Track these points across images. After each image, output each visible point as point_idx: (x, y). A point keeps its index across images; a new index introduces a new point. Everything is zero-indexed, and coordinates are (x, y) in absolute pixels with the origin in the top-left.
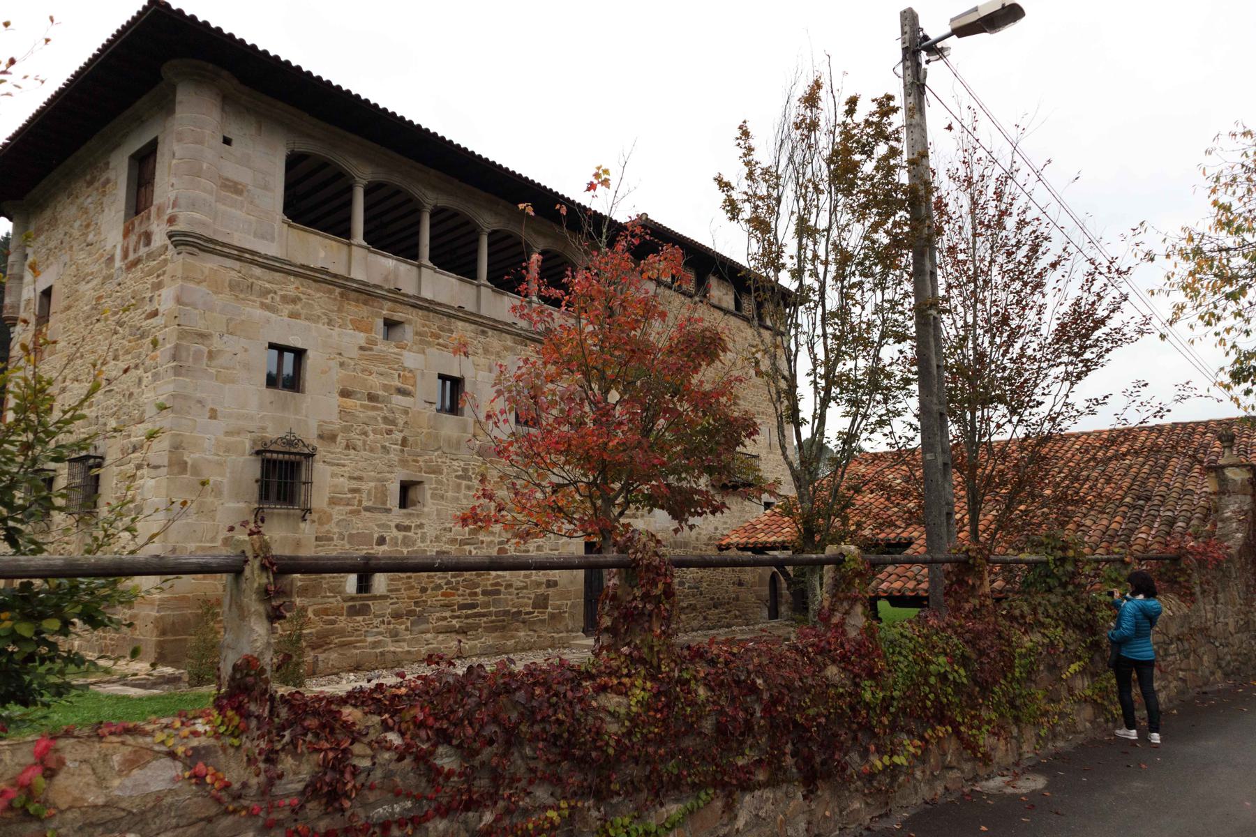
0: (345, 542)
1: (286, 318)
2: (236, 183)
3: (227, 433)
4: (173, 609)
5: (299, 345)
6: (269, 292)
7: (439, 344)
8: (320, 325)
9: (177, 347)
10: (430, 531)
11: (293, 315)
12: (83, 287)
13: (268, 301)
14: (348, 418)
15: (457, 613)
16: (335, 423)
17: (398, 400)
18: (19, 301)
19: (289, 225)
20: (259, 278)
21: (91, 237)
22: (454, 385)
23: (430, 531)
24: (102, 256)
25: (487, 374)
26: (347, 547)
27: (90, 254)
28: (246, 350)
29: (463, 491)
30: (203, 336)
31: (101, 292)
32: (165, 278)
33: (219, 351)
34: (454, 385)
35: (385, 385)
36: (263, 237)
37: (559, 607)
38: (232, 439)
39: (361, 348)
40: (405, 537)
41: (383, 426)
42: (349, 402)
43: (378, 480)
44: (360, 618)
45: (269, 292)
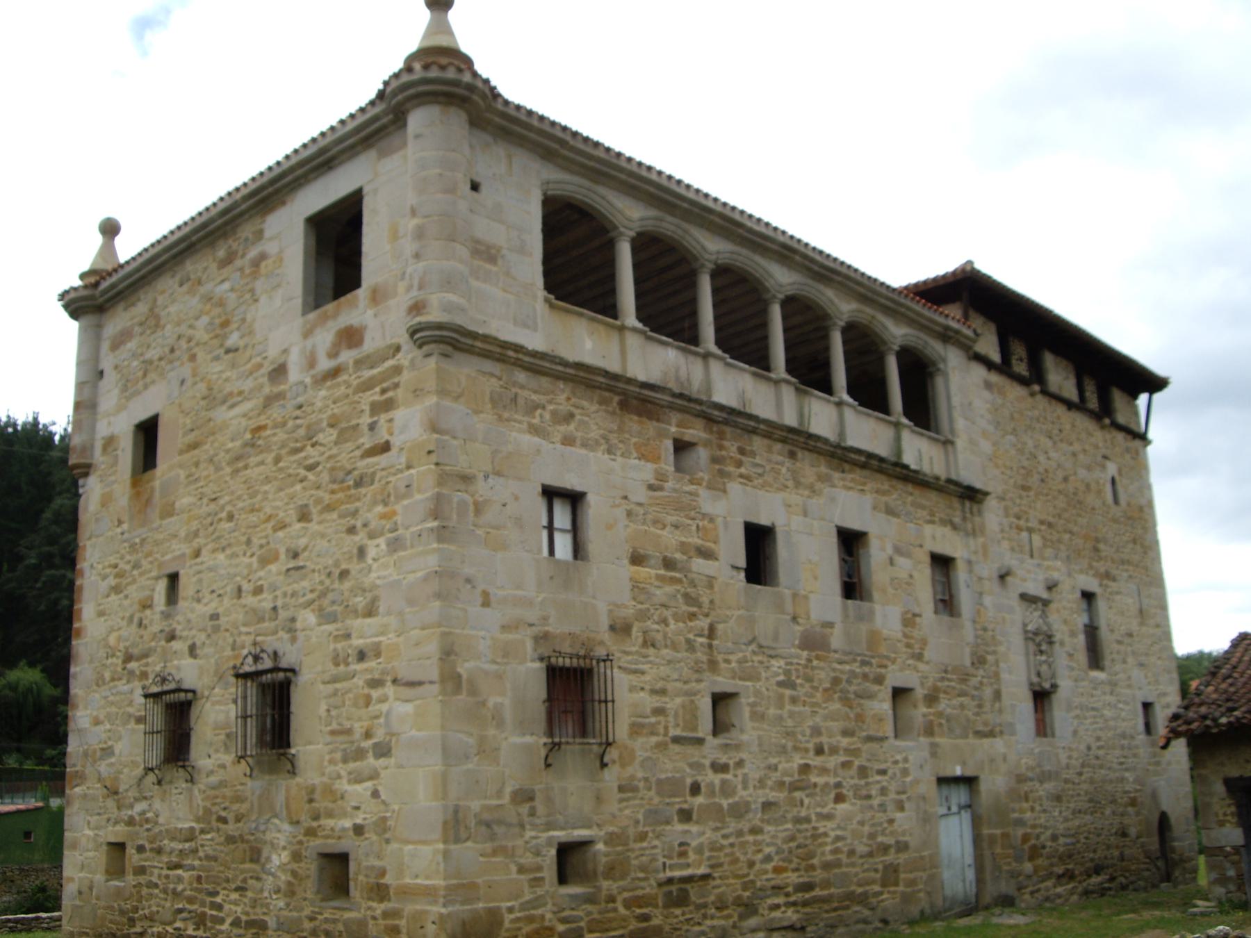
0: (652, 793)
1: (558, 446)
2: (489, 247)
3: (505, 628)
4: (463, 903)
5: (579, 488)
6: (537, 406)
7: (741, 476)
8: (599, 454)
9: (439, 498)
10: (753, 770)
11: (568, 441)
12: (222, 414)
13: (536, 421)
14: (642, 597)
15: (792, 899)
16: (629, 609)
17: (699, 564)
18: (93, 439)
19: (552, 306)
20: (522, 387)
21: (233, 339)
22: (759, 541)
23: (753, 770)
24: (260, 366)
25: (801, 518)
26: (656, 800)
27: (233, 365)
28: (517, 498)
29: (788, 707)
30: (467, 479)
31: (263, 420)
32: (399, 394)
33: (486, 501)
34: (759, 541)
35: (683, 544)
36: (525, 325)
37: (912, 883)
38: (510, 636)
39: (651, 487)
40: (724, 782)
41: (685, 608)
42: (643, 572)
43: (687, 694)
44: (678, 911)
45: (537, 406)
